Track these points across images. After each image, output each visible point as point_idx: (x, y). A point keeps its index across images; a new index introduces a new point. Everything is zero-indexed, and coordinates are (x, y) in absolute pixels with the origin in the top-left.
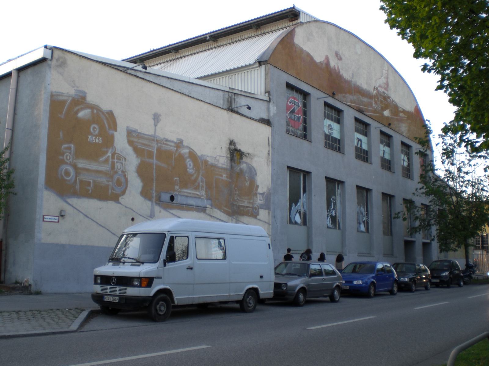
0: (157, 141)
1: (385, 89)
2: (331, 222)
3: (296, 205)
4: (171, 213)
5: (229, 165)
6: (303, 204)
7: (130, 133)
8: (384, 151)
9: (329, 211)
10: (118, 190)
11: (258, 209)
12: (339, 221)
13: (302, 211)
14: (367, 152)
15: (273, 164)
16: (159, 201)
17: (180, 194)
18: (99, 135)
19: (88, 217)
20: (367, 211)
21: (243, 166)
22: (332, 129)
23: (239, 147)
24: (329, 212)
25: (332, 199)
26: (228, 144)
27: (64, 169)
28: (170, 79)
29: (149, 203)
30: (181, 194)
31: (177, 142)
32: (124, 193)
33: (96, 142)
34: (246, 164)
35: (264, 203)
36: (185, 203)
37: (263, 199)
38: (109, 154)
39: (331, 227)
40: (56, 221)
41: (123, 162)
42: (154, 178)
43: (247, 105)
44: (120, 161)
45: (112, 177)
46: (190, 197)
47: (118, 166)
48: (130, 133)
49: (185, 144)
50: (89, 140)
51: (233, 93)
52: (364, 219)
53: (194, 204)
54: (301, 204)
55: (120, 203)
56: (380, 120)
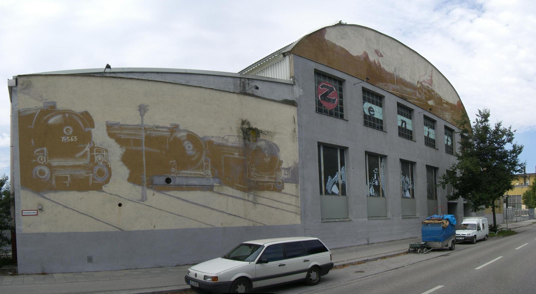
0: (145, 129)
1: (429, 84)
2: (373, 190)
3: (333, 177)
4: (168, 195)
5: (242, 143)
6: (341, 176)
7: (110, 127)
8: (429, 132)
9: (371, 181)
10: (100, 180)
11: (283, 183)
12: (382, 190)
13: (340, 182)
14: (411, 132)
15: (300, 140)
16: (151, 185)
17: (178, 176)
18: (74, 134)
19: (68, 208)
20: (412, 180)
21: (261, 144)
22: (373, 111)
23: (254, 126)
24: (372, 182)
25: (374, 171)
26: (240, 124)
27: (38, 171)
29: (139, 188)
30: (180, 176)
31: (171, 127)
32: (107, 182)
33: (71, 141)
34: (265, 142)
35: (290, 177)
36: (185, 184)
37: (289, 174)
38: (87, 149)
39: (374, 195)
41: (105, 154)
42: (144, 164)
44: (100, 154)
45: (92, 169)
46: (191, 177)
47: (98, 158)
48: (110, 127)
49: (181, 128)
50: (63, 141)
51: (246, 78)
52: (409, 187)
53: (197, 184)
54: (339, 176)
55: (104, 192)
56: (424, 106)
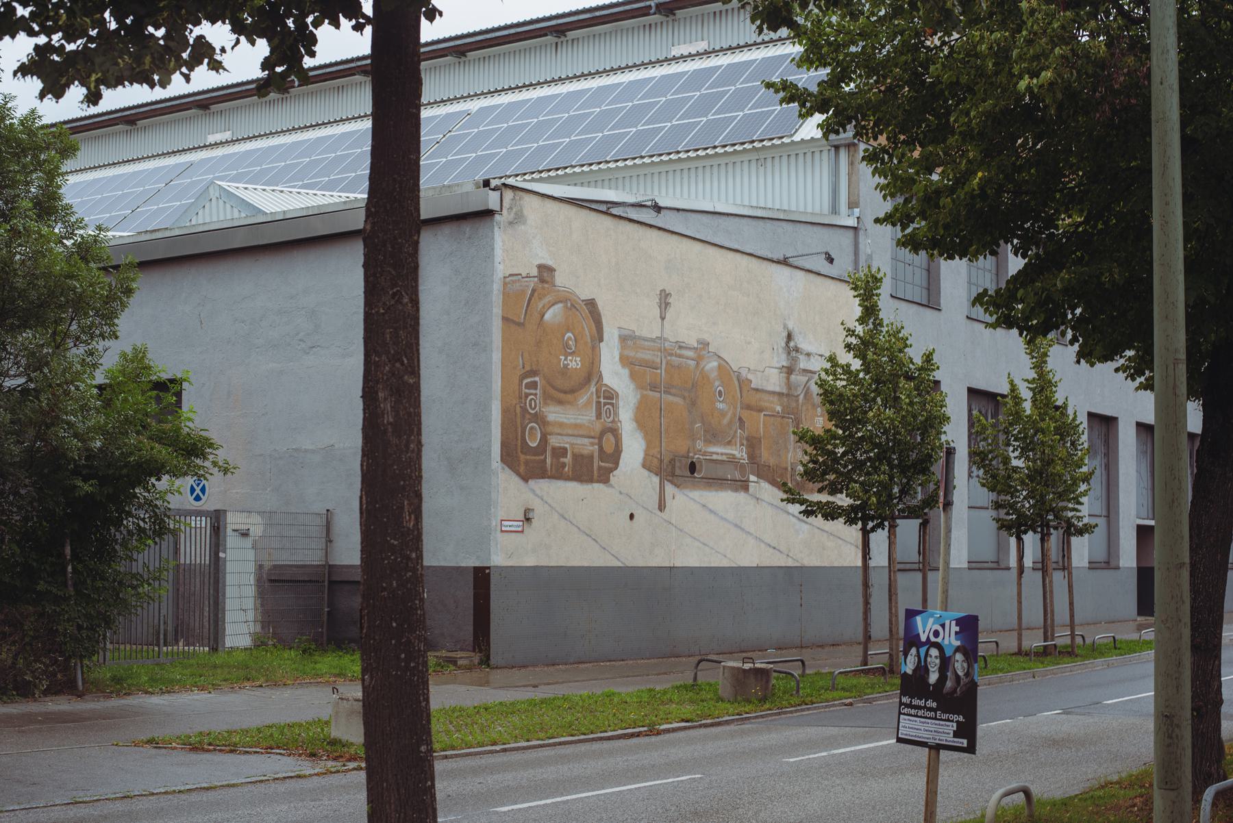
7: (626, 339)
19: (565, 519)
28: (681, 212)
40: (520, 529)
43: (826, 253)
